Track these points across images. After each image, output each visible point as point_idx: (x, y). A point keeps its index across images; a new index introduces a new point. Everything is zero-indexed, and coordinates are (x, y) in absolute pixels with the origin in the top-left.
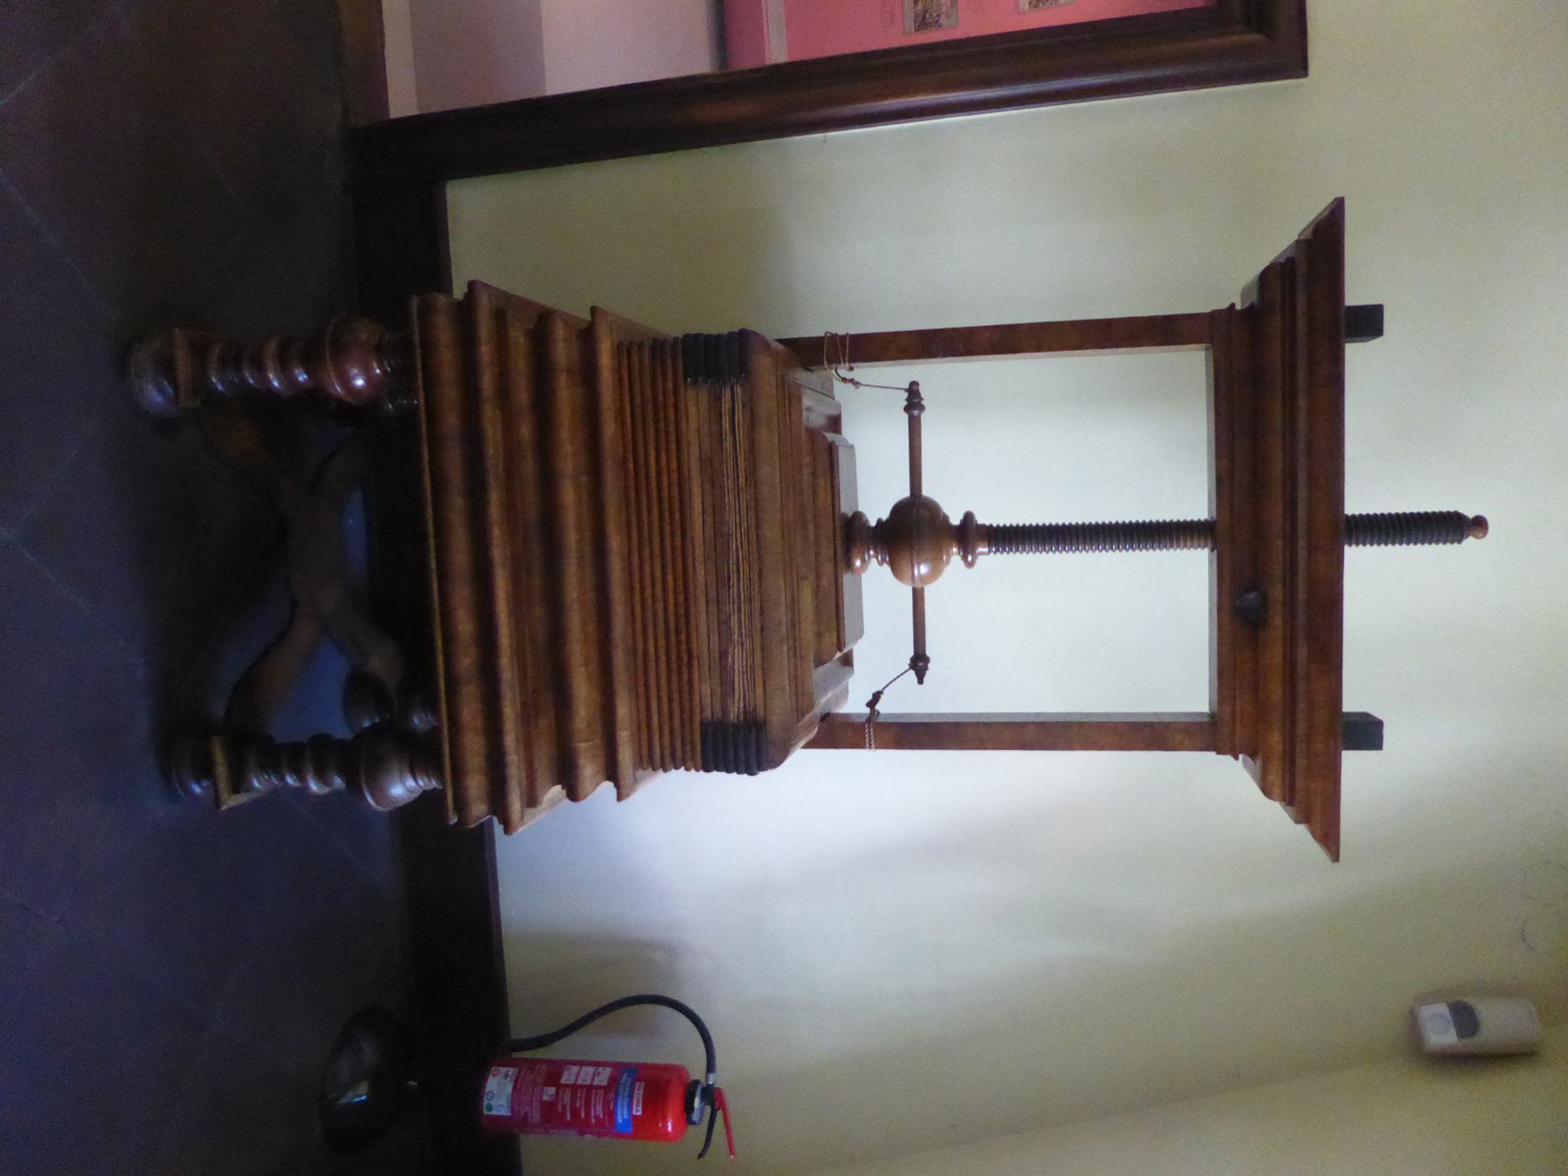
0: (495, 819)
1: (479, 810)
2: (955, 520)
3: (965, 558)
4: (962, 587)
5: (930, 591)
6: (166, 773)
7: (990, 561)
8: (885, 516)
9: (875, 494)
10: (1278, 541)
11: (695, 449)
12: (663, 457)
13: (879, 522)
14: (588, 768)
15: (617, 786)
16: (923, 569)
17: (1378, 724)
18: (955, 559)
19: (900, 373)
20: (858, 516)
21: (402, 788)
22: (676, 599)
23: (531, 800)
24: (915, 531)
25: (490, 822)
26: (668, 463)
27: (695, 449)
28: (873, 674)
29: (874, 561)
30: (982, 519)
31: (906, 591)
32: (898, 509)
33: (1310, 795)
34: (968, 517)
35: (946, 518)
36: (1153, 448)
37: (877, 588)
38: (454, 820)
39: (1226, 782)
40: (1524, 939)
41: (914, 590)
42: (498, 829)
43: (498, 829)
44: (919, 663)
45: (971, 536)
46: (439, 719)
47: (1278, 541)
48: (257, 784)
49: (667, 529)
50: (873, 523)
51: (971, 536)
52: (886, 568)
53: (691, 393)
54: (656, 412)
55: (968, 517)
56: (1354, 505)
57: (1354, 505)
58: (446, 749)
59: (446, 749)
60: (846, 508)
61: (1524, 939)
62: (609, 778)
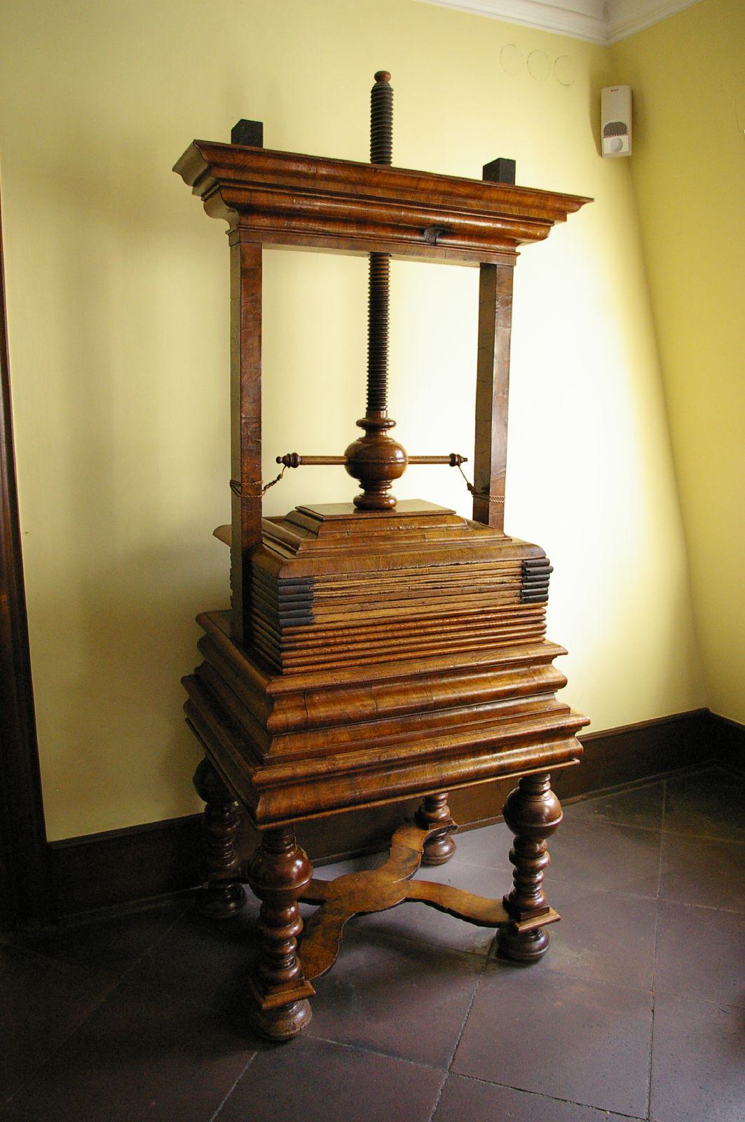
0: (577, 734)
1: (573, 745)
2: (362, 433)
3: (389, 427)
4: (408, 431)
5: (409, 454)
6: (536, 960)
7: (392, 409)
8: (357, 482)
9: (337, 490)
10: (378, 207)
11: (356, 615)
12: (357, 638)
13: (361, 486)
14: (548, 677)
15: (555, 656)
16: (399, 454)
17: (243, 123)
18: (389, 434)
19: (270, 469)
20: (356, 502)
21: (549, 801)
22: (330, 637)
23: (566, 711)
24: (371, 461)
25: (579, 738)
26: (362, 634)
27: (356, 615)
28: (449, 492)
29: (388, 491)
30: (362, 414)
31: (409, 468)
32: (354, 472)
33: (550, 209)
34: (361, 424)
35: (360, 440)
36: (316, 287)
37: (405, 491)
38: (577, 761)
39: (534, 264)
40: (568, 85)
41: (410, 463)
42: (585, 731)
43: (585, 731)
44: (454, 460)
45: (374, 423)
46: (544, 774)
47: (378, 207)
48: (540, 900)
49: (404, 633)
50: (362, 491)
51: (374, 423)
52: (394, 483)
53: (318, 619)
54: (328, 645)
55: (361, 424)
56: (361, 153)
57: (361, 153)
58: (400, 799)
59: (400, 799)
60: (350, 511)
61: (568, 85)
62: (550, 662)
